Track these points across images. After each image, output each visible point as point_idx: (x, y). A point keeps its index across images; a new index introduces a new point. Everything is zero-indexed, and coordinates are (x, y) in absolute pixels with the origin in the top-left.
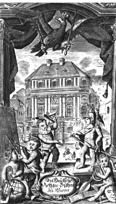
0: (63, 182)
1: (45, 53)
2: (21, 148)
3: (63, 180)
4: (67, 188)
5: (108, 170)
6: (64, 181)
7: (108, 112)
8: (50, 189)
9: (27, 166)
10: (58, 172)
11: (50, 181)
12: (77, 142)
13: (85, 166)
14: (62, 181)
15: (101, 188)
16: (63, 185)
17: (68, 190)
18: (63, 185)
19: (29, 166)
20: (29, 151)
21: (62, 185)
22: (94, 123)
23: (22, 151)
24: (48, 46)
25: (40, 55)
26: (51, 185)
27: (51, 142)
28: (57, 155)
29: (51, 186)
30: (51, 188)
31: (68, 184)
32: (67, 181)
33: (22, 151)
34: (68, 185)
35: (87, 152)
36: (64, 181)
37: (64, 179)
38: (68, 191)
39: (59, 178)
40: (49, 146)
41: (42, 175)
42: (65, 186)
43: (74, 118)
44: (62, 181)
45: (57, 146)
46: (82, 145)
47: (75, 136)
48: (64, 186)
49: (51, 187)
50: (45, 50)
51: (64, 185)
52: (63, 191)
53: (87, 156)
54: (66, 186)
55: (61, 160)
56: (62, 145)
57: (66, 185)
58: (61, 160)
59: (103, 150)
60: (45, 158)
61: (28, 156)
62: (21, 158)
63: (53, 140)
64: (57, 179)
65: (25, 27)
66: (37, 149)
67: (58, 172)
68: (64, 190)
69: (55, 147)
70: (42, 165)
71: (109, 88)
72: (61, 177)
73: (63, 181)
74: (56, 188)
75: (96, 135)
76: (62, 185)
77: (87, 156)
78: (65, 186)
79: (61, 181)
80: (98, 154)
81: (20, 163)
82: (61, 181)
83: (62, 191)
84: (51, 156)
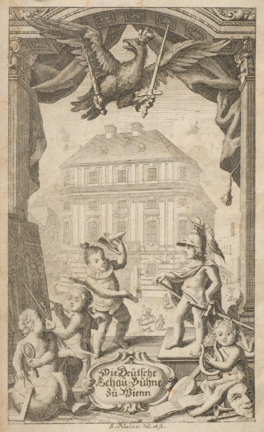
0: (139, 375)
1: (102, 112)
2: (52, 306)
3: (138, 372)
4: (145, 389)
5: (233, 352)
6: (140, 373)
7: (233, 235)
8: (112, 390)
9: (64, 344)
10: (128, 355)
11: (110, 374)
12: (167, 295)
13: (182, 344)
14: (137, 374)
15: (218, 388)
16: (138, 382)
17: (149, 392)
18: (138, 382)
19: (67, 342)
20: (69, 312)
21: (136, 382)
22: (201, 257)
23: (53, 313)
24: (108, 98)
25: (93, 114)
26: (150, 373)
27: (114, 293)
28: (124, 324)
29: (150, 374)
30: (114, 388)
31: (148, 380)
32: (146, 374)
33: (53, 313)
34: (149, 382)
35: (188, 316)
36: (140, 373)
37: (140, 371)
38: (148, 394)
39: (129, 367)
40: (109, 301)
41: (94, 362)
42: (143, 384)
43: (142, 275)
44: (137, 374)
45: (126, 302)
46: (177, 300)
47: (163, 282)
48: (140, 383)
49: (114, 386)
50: (103, 105)
51: (141, 381)
52: (139, 394)
53: (187, 324)
54: (145, 385)
55: (133, 330)
56: (136, 300)
57: (144, 381)
58: (133, 330)
59: (221, 311)
60: (102, 326)
61: (66, 321)
62: (53, 325)
63: (118, 290)
64: (125, 368)
65: (62, 61)
66: (85, 310)
67: (128, 355)
68: (139, 393)
69: (123, 307)
70: (95, 342)
71: (234, 184)
72: (134, 366)
73: (138, 373)
74: (124, 388)
75: (206, 283)
76: (136, 382)
77: (187, 324)
78: (143, 384)
79: (133, 374)
80: (210, 320)
81: (47, 336)
82: (133, 374)
83: (135, 394)
84: (115, 321)
